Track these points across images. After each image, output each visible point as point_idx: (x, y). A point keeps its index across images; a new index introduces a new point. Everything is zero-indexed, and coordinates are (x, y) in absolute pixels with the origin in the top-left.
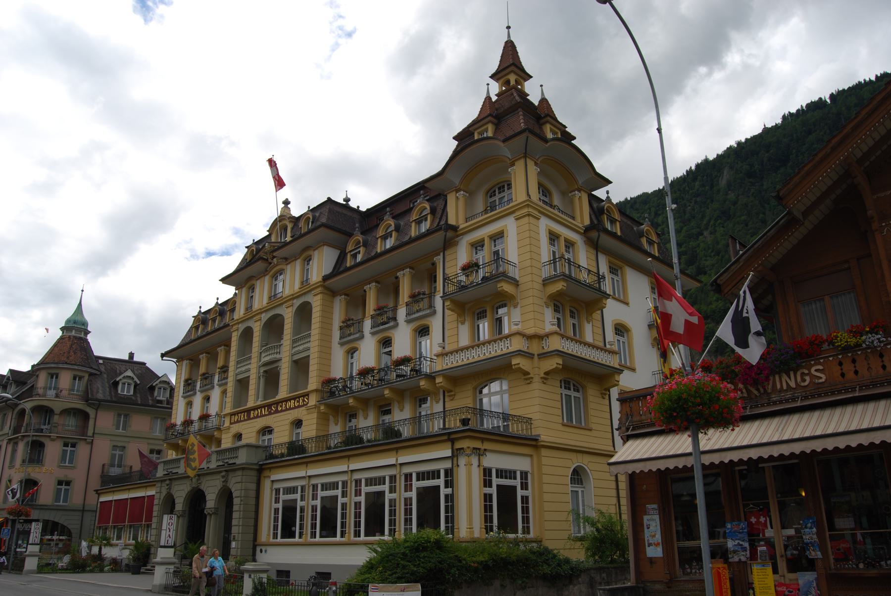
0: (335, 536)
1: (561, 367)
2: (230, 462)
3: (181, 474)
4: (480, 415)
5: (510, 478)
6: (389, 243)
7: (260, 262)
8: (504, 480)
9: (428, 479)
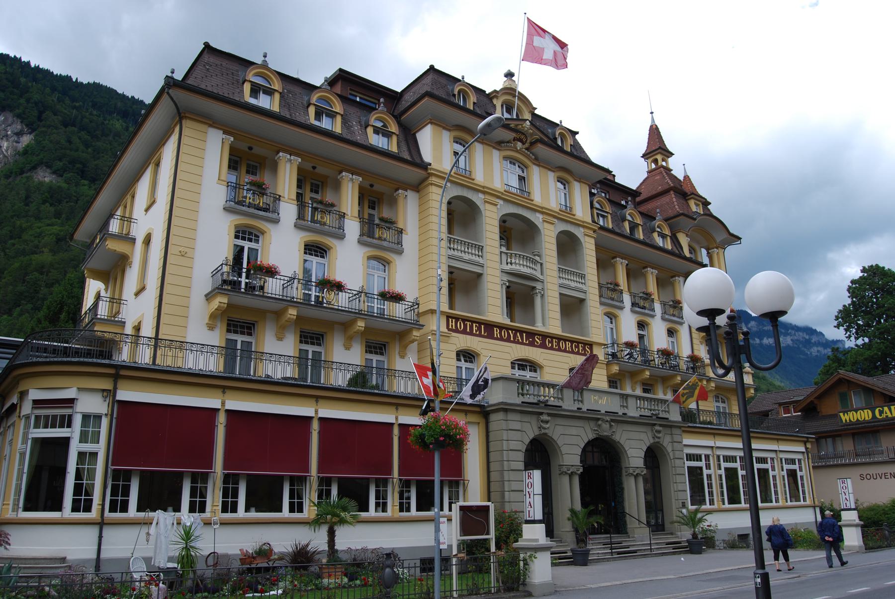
2: (661, 416)
4: (388, 375)
5: (697, 461)
7: (426, 99)
8: (692, 462)
9: (53, 426)
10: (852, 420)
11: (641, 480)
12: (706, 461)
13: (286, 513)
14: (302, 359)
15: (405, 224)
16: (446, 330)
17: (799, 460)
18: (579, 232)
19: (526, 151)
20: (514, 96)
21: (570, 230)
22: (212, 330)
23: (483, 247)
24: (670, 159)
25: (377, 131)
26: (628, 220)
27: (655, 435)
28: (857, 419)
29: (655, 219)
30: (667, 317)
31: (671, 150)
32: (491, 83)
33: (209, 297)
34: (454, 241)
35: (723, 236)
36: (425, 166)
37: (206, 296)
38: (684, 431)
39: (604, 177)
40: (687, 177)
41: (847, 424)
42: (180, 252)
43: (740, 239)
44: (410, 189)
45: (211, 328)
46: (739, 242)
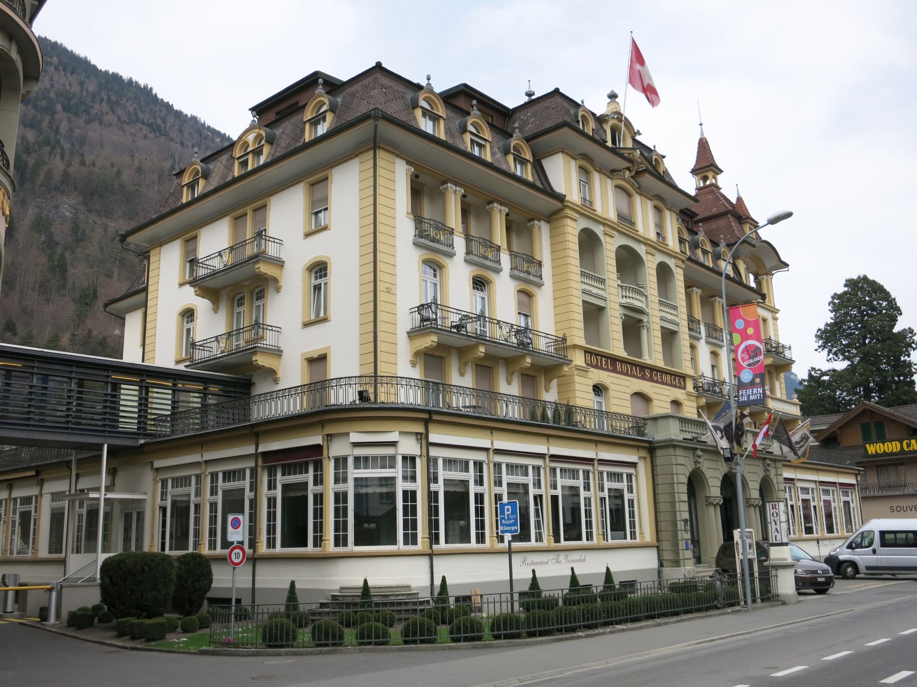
0: (305, 544)
1: (436, 344)
3: (775, 456)
6: (322, 129)
10: (878, 451)
11: (758, 509)
12: (628, 482)
13: (473, 544)
14: (477, 392)
15: (541, 255)
16: (585, 365)
17: (813, 490)
18: (671, 263)
19: (632, 180)
20: (620, 120)
21: (590, 227)
22: (414, 367)
23: (605, 280)
24: (719, 177)
25: (425, 113)
26: (422, 108)
27: (697, 460)
28: (884, 450)
29: (469, 114)
30: (711, 340)
31: (720, 166)
32: (599, 107)
33: (412, 334)
34: (626, 289)
35: (776, 262)
36: (560, 198)
37: (408, 333)
38: (784, 466)
39: (685, 207)
40: (739, 199)
41: (872, 456)
42: (387, 288)
43: (787, 265)
44: (544, 220)
45: (414, 364)
46: (786, 269)
